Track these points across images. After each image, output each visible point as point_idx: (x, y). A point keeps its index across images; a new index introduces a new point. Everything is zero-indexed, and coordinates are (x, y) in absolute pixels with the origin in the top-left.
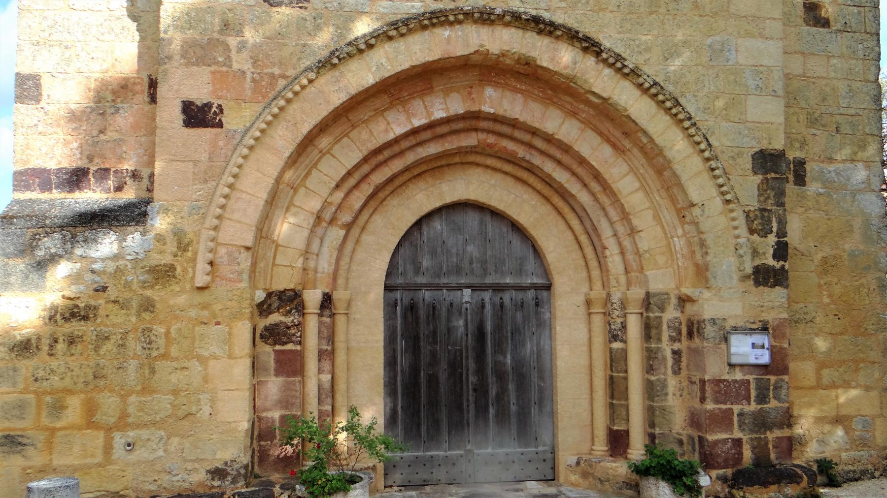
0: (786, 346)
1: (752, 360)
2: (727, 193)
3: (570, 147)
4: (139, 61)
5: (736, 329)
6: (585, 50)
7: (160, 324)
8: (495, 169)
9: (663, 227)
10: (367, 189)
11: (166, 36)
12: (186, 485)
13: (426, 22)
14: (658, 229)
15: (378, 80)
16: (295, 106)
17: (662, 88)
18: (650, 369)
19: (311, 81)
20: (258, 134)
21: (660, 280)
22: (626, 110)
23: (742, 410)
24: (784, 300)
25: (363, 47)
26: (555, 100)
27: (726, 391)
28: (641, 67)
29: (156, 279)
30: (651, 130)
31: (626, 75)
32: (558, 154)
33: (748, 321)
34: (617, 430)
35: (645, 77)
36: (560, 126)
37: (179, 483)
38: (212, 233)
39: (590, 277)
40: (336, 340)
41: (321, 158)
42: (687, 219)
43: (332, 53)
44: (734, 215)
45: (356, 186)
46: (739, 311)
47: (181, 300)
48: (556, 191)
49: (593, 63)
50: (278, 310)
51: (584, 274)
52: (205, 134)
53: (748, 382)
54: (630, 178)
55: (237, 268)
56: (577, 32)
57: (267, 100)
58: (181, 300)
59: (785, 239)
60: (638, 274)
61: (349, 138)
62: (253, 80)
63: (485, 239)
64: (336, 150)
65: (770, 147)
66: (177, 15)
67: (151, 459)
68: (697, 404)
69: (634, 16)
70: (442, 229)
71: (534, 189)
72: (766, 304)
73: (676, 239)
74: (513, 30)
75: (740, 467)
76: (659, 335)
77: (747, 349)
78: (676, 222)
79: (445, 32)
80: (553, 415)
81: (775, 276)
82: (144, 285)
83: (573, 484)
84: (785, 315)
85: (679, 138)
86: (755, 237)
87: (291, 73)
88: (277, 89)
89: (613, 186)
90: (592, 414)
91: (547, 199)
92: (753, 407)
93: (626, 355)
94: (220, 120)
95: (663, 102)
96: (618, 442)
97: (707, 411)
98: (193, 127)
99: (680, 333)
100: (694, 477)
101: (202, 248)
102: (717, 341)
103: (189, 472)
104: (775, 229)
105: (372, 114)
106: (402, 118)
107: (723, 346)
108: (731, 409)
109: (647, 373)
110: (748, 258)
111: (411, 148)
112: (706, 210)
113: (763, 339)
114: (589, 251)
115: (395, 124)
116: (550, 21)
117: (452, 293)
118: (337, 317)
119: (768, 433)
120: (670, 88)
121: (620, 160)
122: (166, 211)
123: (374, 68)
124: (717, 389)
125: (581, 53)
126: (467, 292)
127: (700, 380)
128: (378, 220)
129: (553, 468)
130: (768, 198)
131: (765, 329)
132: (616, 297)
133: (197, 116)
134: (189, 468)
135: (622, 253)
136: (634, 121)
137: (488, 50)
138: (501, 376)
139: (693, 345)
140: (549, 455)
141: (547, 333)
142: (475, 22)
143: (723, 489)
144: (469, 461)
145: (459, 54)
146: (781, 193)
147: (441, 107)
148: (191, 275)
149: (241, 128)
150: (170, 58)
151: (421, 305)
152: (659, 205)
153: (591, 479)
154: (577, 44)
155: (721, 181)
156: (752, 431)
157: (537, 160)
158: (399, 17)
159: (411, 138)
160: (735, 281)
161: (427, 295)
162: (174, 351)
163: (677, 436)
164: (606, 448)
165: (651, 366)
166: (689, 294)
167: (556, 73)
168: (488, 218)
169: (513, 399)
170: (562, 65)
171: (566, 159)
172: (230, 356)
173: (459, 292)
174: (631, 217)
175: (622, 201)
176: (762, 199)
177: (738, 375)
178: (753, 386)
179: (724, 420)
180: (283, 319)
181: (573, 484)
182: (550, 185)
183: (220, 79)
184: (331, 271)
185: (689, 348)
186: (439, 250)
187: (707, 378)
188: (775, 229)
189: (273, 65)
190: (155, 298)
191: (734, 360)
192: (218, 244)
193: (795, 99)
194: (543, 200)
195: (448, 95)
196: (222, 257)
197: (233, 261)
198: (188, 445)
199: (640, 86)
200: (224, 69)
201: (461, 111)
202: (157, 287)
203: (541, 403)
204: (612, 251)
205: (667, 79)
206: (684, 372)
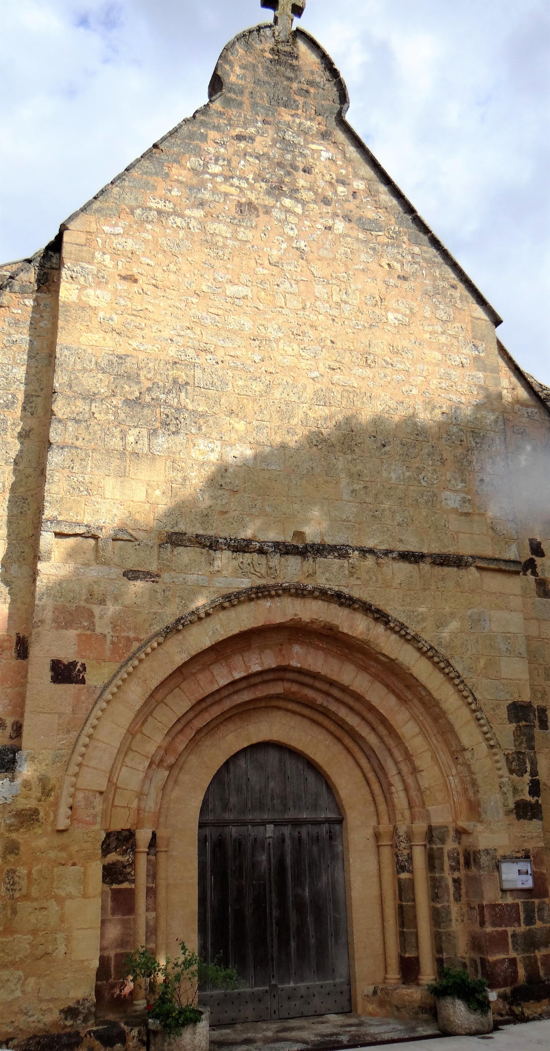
0: (545, 871)
1: (520, 886)
2: (491, 739)
3: (363, 697)
4: (9, 620)
5: (505, 858)
6: (376, 620)
7: (22, 865)
8: (294, 712)
9: (440, 767)
10: (190, 733)
11: (41, 603)
12: (41, 1026)
13: (253, 596)
14: (436, 768)
15: (213, 643)
16: (145, 665)
17: (436, 651)
18: (435, 897)
19: (159, 644)
20: (115, 690)
21: (440, 816)
22: (409, 669)
23: (514, 931)
24: (540, 830)
25: (203, 615)
26: (350, 657)
27: (503, 915)
28: (419, 633)
29: (22, 823)
30: (430, 686)
31: (408, 641)
32: (351, 702)
33: (513, 851)
34: (409, 958)
35: (423, 642)
36: (354, 679)
37: (35, 1024)
38: (73, 779)
39: (377, 810)
40: (158, 877)
41: (156, 706)
42: (460, 761)
43: (178, 620)
44: (497, 758)
45: (181, 731)
46: (506, 842)
47: (42, 842)
48: (347, 732)
49: (383, 630)
50: (116, 850)
51: (372, 809)
52: (71, 689)
53: (517, 905)
54: (411, 724)
55: (92, 811)
56: (371, 606)
57: (123, 660)
58: (42, 842)
59: (537, 777)
60: (421, 809)
61: (180, 688)
62: (113, 643)
63: (285, 776)
64: (169, 700)
65: (520, 700)
66: (51, 585)
67: (9, 1000)
68: (477, 928)
69: (412, 592)
70: (247, 767)
71: (327, 730)
72: (526, 835)
73: (451, 778)
74: (320, 602)
75: (516, 985)
76: (442, 864)
77: (515, 876)
78: (451, 763)
79: (268, 603)
80: (348, 945)
81: (531, 810)
82: (10, 828)
83: (370, 1014)
84: (542, 844)
85: (451, 693)
86: (514, 776)
87: (143, 636)
88: (132, 651)
89: (398, 731)
90: (384, 943)
91: (339, 740)
92: (523, 928)
93: (413, 884)
94: (83, 677)
95: (438, 663)
96: (409, 969)
97: (486, 934)
98: (60, 683)
99: (458, 863)
100: (484, 994)
101: (65, 793)
102: (491, 869)
103: (43, 1012)
104: (528, 769)
105: (200, 667)
106: (225, 671)
107: (496, 874)
108: (506, 931)
109: (433, 900)
110: (510, 795)
111: (228, 696)
112: (475, 754)
113: (526, 866)
114: (376, 787)
115: (222, 676)
116: (350, 596)
117: (256, 828)
118: (159, 855)
119: (536, 951)
120: (442, 651)
121: (403, 708)
122: (33, 759)
123: (210, 633)
124: (493, 913)
125: (373, 622)
126: (270, 828)
127: (479, 906)
128: (193, 760)
129: (350, 1000)
130: (521, 743)
131: (527, 857)
132: (402, 830)
133: (64, 673)
134: (44, 1008)
135: (406, 789)
136: (415, 678)
137: (301, 619)
138: (300, 906)
139: (470, 874)
140: (346, 987)
141: (340, 865)
142: (291, 595)
143: (504, 1006)
144: (274, 996)
145: (278, 622)
146: (531, 739)
147: (257, 661)
148: (52, 818)
149: (100, 684)
150: (42, 622)
151: (229, 838)
152: (436, 747)
153: (388, 1007)
154: (371, 615)
155: (485, 729)
156: (524, 951)
157: (333, 707)
158: (231, 591)
159: (229, 687)
160: (501, 815)
161: (234, 831)
162: (34, 892)
163: (461, 960)
164: (399, 976)
165: (436, 894)
166: (465, 826)
167: (354, 637)
168: (286, 756)
169: (312, 933)
170: (359, 632)
171: (357, 706)
172: (85, 896)
173: (262, 828)
174: (414, 758)
175: (406, 744)
176: (517, 743)
177: (509, 900)
178: (521, 908)
179: (499, 941)
180: (120, 858)
181: (370, 1014)
182: (342, 728)
183: (85, 641)
184: (157, 810)
185: (467, 876)
186: (244, 787)
187: (485, 903)
188: (528, 769)
189: (129, 629)
190: (20, 840)
191: (506, 886)
192: (77, 789)
193: (535, 657)
194: (335, 741)
195: (263, 652)
196: (79, 802)
197: (89, 804)
198: (44, 985)
199: (419, 649)
200: (89, 632)
201: (274, 666)
202: (21, 830)
203: (337, 934)
204: (397, 786)
205: (440, 644)
206: (464, 899)
